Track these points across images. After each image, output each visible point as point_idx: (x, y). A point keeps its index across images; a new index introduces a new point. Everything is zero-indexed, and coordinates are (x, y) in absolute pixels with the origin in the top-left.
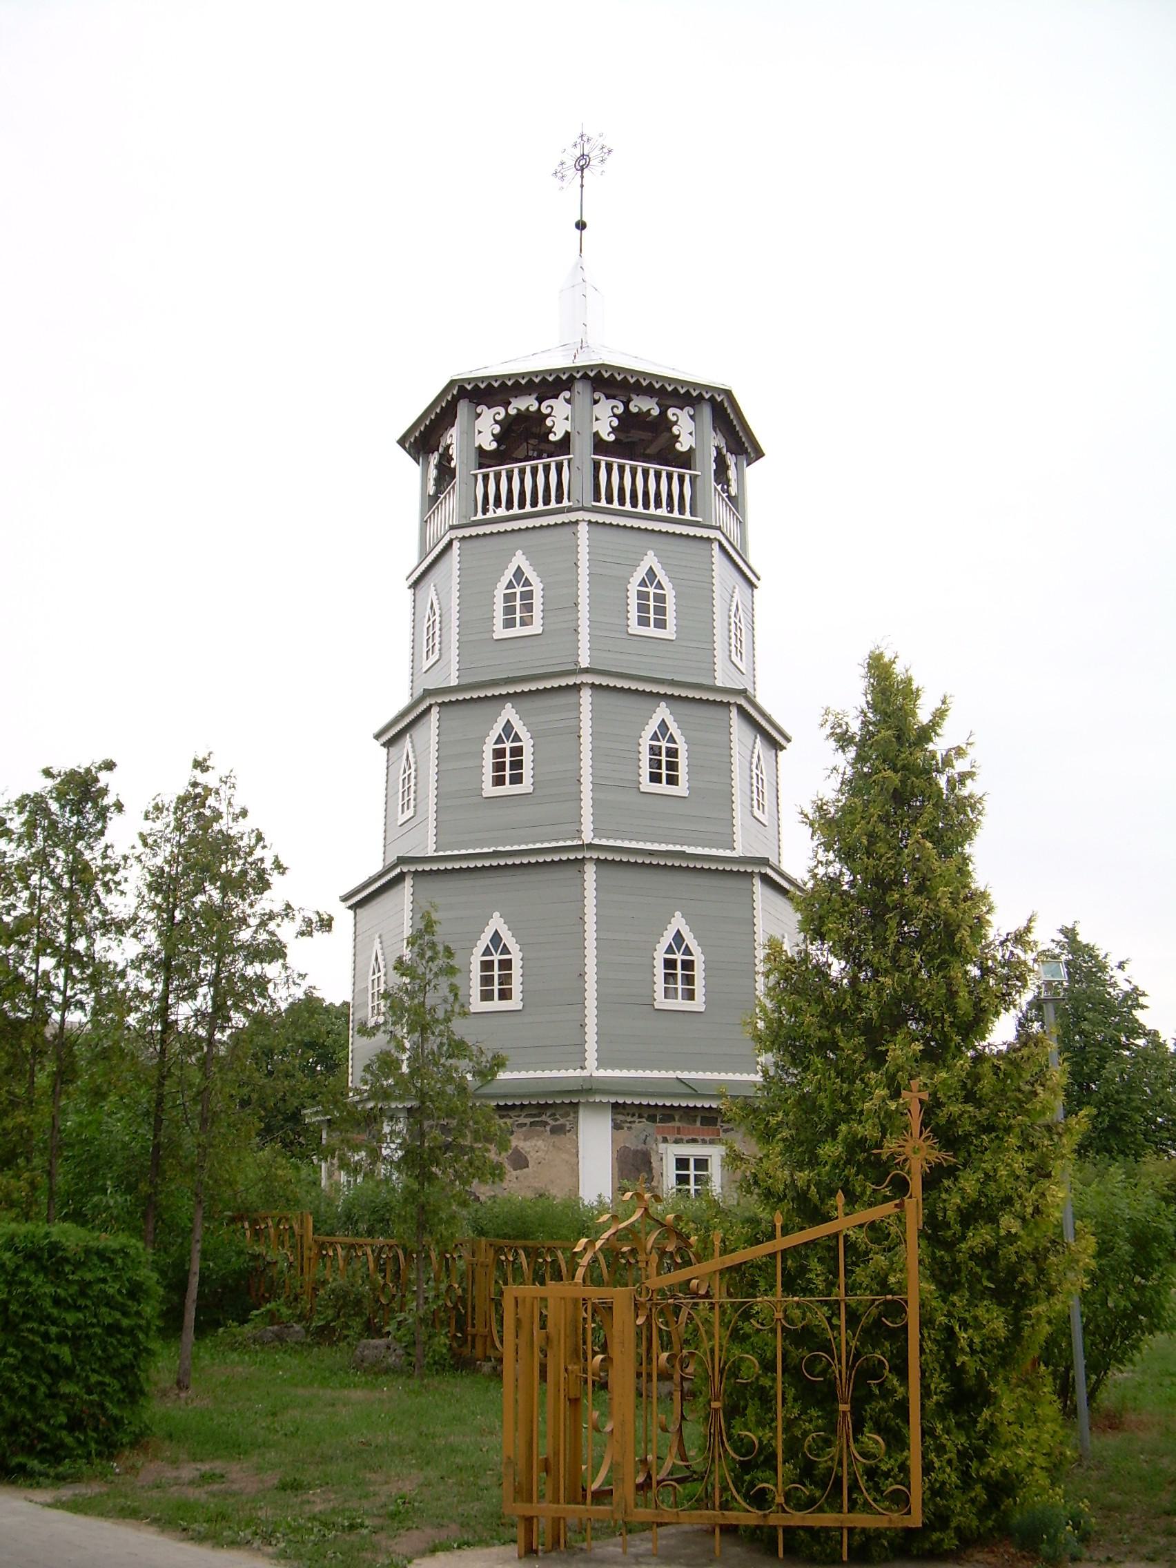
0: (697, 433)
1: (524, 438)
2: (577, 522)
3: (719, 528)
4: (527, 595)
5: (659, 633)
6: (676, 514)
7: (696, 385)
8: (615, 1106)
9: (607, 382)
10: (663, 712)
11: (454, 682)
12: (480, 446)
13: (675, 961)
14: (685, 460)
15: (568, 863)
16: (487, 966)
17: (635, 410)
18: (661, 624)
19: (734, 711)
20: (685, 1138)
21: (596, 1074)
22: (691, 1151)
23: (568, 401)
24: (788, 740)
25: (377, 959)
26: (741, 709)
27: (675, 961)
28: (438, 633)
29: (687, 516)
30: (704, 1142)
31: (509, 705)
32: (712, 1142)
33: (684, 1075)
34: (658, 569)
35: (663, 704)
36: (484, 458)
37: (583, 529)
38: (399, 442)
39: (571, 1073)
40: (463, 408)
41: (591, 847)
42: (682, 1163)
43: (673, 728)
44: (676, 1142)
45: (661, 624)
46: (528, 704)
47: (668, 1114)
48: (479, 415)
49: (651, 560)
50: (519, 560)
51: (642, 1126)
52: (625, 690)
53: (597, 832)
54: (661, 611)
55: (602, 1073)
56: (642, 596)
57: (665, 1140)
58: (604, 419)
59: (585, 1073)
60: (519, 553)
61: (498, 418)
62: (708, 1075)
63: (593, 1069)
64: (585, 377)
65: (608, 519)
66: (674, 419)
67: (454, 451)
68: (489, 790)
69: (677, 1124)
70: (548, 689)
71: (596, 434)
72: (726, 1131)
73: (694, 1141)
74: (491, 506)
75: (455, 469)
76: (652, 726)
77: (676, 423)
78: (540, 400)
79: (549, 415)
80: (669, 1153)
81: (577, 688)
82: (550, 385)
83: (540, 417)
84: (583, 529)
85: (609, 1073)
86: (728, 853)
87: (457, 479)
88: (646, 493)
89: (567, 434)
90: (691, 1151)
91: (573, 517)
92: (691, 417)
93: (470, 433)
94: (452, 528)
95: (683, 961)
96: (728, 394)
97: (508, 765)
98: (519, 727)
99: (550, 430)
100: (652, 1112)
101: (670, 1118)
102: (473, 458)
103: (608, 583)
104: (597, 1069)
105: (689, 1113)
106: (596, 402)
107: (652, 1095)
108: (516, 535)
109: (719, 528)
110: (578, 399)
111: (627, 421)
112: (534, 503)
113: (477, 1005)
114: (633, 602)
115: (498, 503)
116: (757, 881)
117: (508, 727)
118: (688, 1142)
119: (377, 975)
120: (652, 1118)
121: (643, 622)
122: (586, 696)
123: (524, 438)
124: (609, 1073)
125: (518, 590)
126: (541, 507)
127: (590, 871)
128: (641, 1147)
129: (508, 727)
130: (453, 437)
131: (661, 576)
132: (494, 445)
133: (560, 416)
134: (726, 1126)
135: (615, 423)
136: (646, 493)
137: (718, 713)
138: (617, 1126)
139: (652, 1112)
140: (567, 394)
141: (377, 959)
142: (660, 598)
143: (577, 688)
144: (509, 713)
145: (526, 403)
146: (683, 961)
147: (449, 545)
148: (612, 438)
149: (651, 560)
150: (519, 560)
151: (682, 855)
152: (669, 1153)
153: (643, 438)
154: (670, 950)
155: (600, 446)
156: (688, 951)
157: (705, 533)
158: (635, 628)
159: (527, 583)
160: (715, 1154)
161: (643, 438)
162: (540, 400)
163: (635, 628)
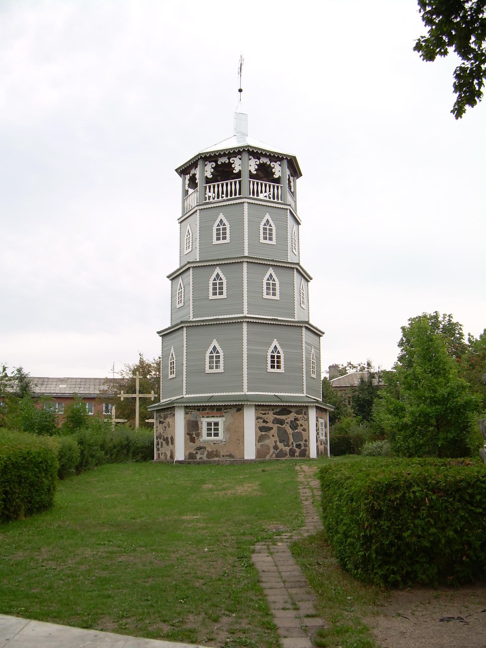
0: (283, 171)
2: (243, 203)
3: (290, 205)
4: (224, 229)
6: (272, 200)
7: (281, 154)
8: (186, 407)
9: (255, 153)
10: (271, 271)
11: (198, 260)
12: (206, 176)
13: (274, 356)
14: (278, 181)
15: (237, 323)
16: (218, 230)
17: (262, 162)
18: (271, 239)
19: (295, 270)
20: (210, 416)
21: (247, 393)
22: (212, 420)
23: (240, 159)
24: (311, 279)
25: (172, 355)
26: (297, 269)
27: (274, 356)
28: (191, 242)
29: (280, 201)
30: (217, 417)
31: (218, 268)
32: (220, 417)
33: (277, 394)
34: (270, 220)
35: (271, 268)
36: (208, 181)
37: (246, 205)
39: (239, 393)
40: (200, 163)
41: (246, 317)
42: (209, 424)
43: (274, 276)
44: (207, 417)
45: (271, 239)
46: (224, 267)
47: (204, 408)
48: (206, 165)
49: (267, 217)
50: (221, 216)
51: (195, 412)
52: (258, 264)
53: (194, 317)
54: (271, 234)
55: (249, 393)
56: (265, 229)
57: (203, 417)
58: (253, 165)
59: (243, 393)
60: (221, 214)
61: (213, 166)
62: (287, 394)
63: (246, 392)
65: (254, 202)
66: (273, 166)
67: (197, 176)
69: (207, 411)
70: (232, 263)
71: (250, 171)
72: (225, 413)
73: (213, 416)
75: (197, 184)
76: (267, 276)
77: (274, 168)
79: (233, 163)
80: (204, 421)
81: (242, 262)
83: (230, 164)
84: (246, 205)
85: (190, 396)
86: (293, 320)
87: (198, 187)
88: (253, 185)
89: (240, 171)
90: (212, 420)
92: (280, 165)
93: (203, 171)
94: (197, 206)
95: (277, 356)
96: (295, 158)
98: (222, 275)
99: (234, 169)
100: (199, 408)
101: (205, 409)
102: (204, 180)
103: (254, 224)
104: (247, 391)
105: (212, 407)
106: (250, 159)
107: (197, 402)
108: (227, 207)
109: (290, 205)
110: (243, 158)
112: (235, 195)
114: (262, 231)
115: (224, 196)
116: (304, 329)
117: (218, 275)
118: (212, 417)
119: (172, 361)
120: (198, 410)
121: (265, 238)
122: (245, 265)
124: (190, 396)
125: (221, 227)
126: (233, 197)
127: (245, 326)
128: (195, 419)
129: (218, 275)
130: (197, 172)
131: (271, 222)
132: (211, 176)
133: (237, 165)
134: (225, 411)
135: (256, 167)
137: (290, 272)
138: (186, 413)
139: (199, 408)
140: (240, 157)
141: (172, 355)
142: (271, 230)
143: (242, 262)
144: (218, 270)
146: (277, 356)
147: (196, 211)
148: (255, 172)
149: (267, 217)
150: (221, 216)
151: (277, 320)
152: (204, 421)
153: (264, 173)
154: (273, 352)
155: (251, 176)
156: (279, 352)
157: (284, 207)
158: (262, 241)
159: (224, 225)
160: (220, 420)
161: (264, 173)
163: (262, 241)
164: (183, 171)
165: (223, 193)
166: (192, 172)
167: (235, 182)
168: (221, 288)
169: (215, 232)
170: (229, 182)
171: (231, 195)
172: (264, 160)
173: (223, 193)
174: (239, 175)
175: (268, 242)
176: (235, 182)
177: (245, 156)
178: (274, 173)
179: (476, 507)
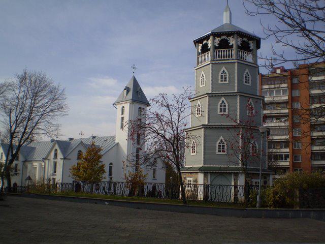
1: (224, 45)
5: (248, 84)
9: (240, 34)
10: (223, 99)
16: (222, 76)
34: (248, 72)
36: (216, 48)
38: (194, 41)
45: (248, 83)
49: (247, 70)
50: (224, 68)
64: (237, 33)
68: (217, 153)
74: (217, 57)
78: (227, 37)
82: (229, 34)
88: (219, 55)
91: (234, 61)
97: (223, 108)
98: (225, 101)
111: (243, 42)
113: (220, 82)
123: (224, 45)
133: (232, 41)
136: (219, 55)
144: (223, 99)
145: (224, 37)
150: (224, 68)
151: (224, 125)
162: (227, 37)
164: (197, 42)
165: (216, 56)
166: (205, 42)
167: (226, 51)
168: (225, 109)
169: (220, 77)
170: (225, 50)
171: (224, 58)
172: (245, 39)
173: (216, 56)
174: (232, 47)
175: (247, 84)
176: (226, 51)
177: (236, 36)
178: (250, 47)
179: (256, 202)
